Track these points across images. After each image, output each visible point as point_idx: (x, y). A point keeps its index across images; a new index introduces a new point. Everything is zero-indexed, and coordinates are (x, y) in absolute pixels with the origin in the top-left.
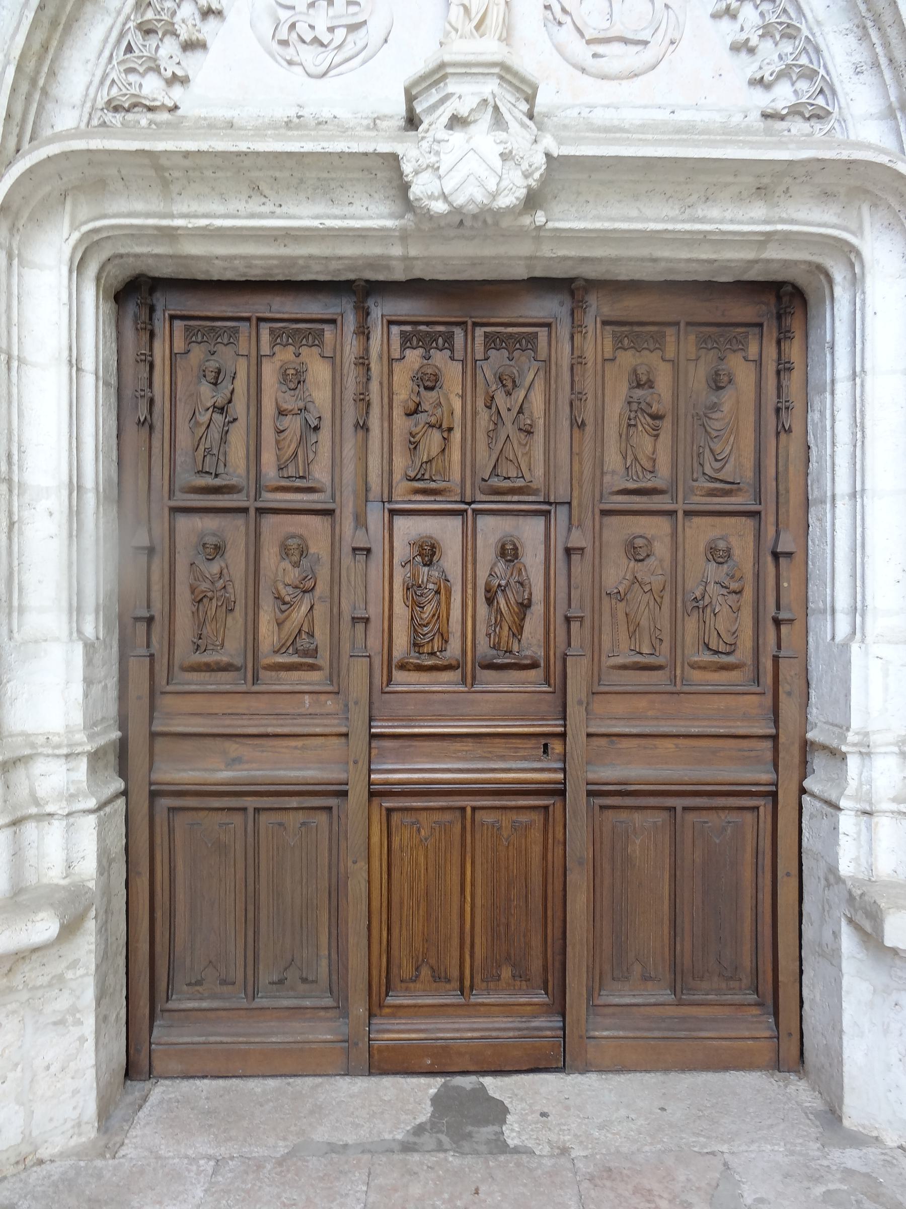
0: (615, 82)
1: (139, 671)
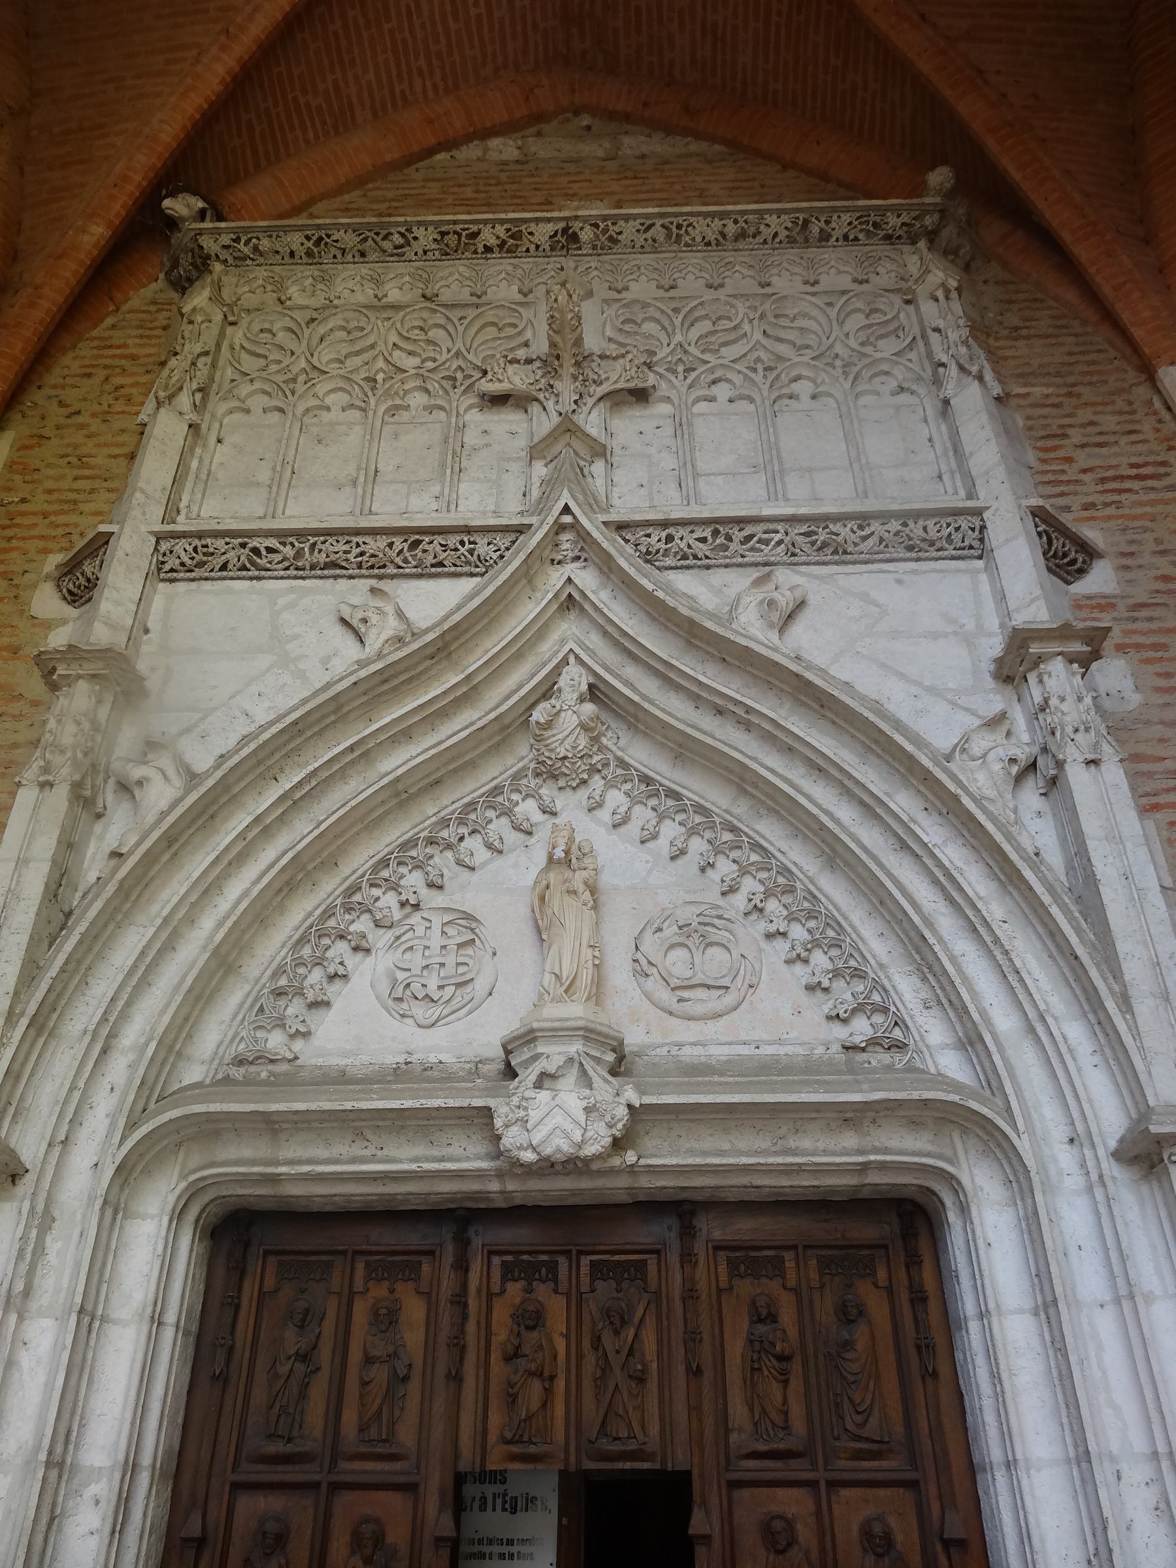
0: (701, 1022)
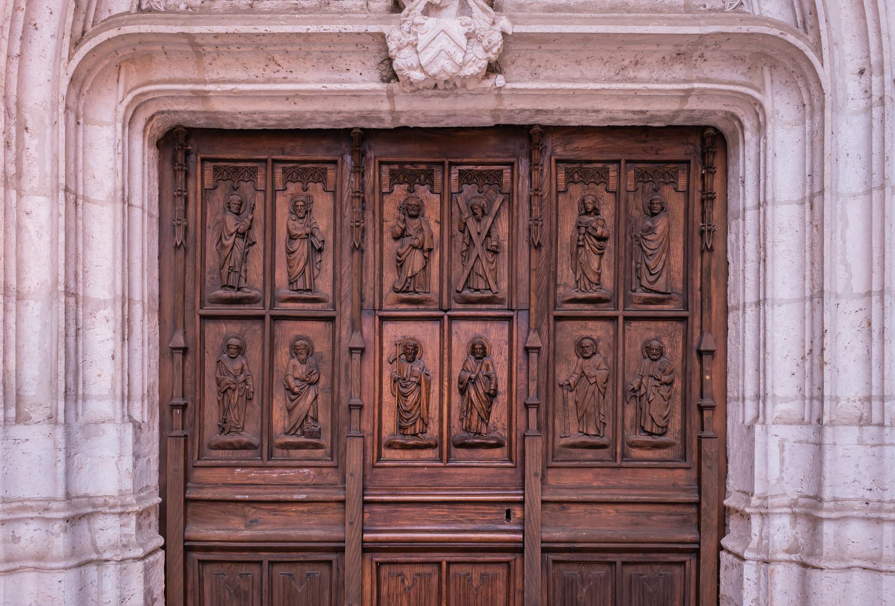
1: (176, 450)
